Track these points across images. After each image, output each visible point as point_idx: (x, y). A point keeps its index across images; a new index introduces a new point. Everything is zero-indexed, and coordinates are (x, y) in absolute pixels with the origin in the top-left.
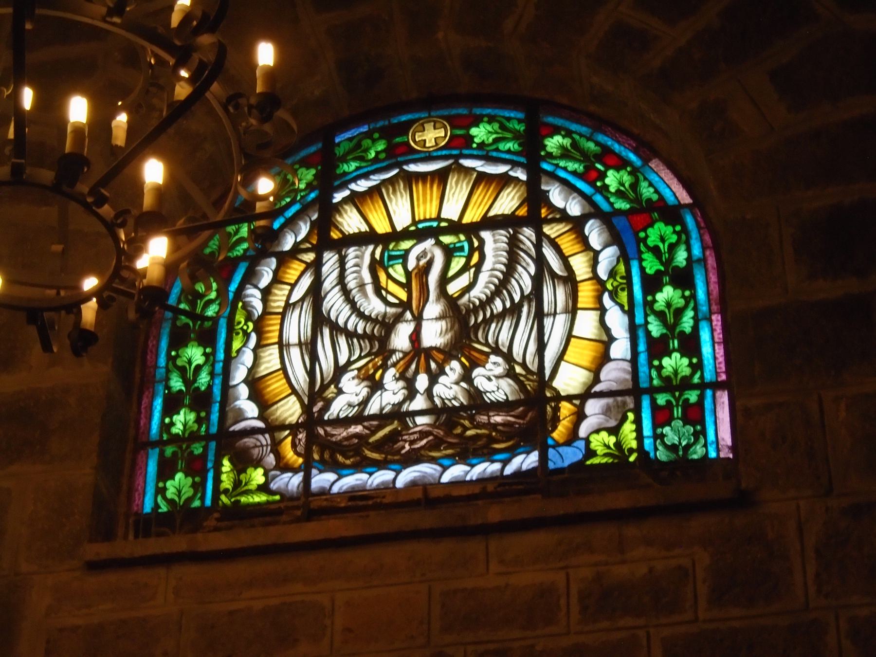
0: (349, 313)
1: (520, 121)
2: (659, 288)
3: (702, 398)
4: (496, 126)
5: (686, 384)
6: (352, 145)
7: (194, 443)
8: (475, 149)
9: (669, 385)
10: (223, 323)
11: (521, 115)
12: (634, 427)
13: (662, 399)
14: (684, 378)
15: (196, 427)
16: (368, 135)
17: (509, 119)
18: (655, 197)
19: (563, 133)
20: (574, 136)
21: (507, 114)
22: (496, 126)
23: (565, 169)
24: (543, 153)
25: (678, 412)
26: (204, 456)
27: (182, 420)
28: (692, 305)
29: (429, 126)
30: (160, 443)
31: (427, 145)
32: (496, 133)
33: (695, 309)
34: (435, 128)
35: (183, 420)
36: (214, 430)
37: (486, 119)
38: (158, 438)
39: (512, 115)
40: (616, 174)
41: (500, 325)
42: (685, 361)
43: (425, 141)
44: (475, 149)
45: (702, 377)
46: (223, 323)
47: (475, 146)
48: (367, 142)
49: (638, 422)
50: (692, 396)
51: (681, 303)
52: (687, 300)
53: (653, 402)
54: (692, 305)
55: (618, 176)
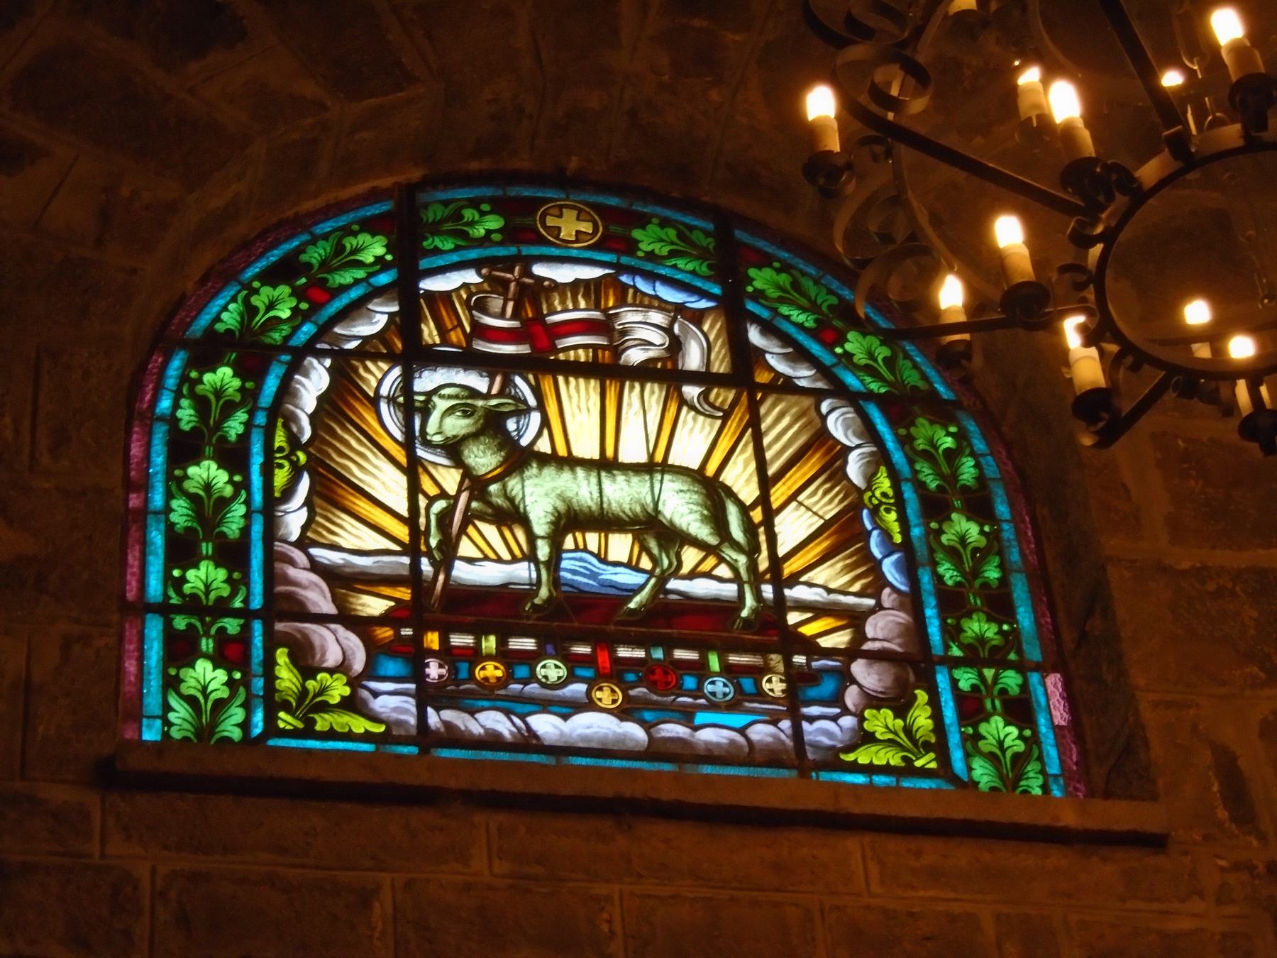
0: (594, 480)
1: (707, 234)
2: (196, 459)
3: (246, 628)
4: (672, 233)
5: (222, 608)
6: (447, 211)
7: (1005, 670)
8: (640, 258)
9: (193, 605)
10: (257, 448)
11: (710, 227)
12: (928, 711)
13: (180, 623)
14: (220, 599)
15: (226, 591)
16: (474, 203)
17: (691, 228)
18: (921, 384)
19: (776, 265)
20: (795, 272)
21: (688, 220)
22: (672, 233)
23: (787, 318)
24: (750, 289)
25: (207, 645)
26: (244, 638)
27: (205, 576)
28: (244, 495)
29: (570, 215)
30: (165, 609)
31: (562, 235)
32: (672, 243)
33: (248, 503)
34: (578, 219)
35: (203, 577)
36: (257, 602)
37: (655, 220)
38: (160, 599)
39: (696, 223)
40: (860, 338)
41: (363, 507)
42: (221, 574)
43: (559, 229)
44: (640, 258)
45: (246, 601)
46: (257, 448)
47: (640, 254)
48: (469, 214)
49: (935, 703)
50: (232, 626)
51: (228, 491)
52: (237, 487)
53: (168, 626)
54: (244, 495)
55: (864, 343)
